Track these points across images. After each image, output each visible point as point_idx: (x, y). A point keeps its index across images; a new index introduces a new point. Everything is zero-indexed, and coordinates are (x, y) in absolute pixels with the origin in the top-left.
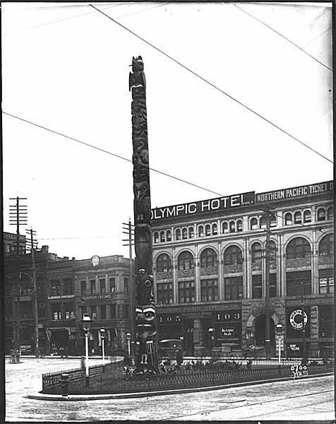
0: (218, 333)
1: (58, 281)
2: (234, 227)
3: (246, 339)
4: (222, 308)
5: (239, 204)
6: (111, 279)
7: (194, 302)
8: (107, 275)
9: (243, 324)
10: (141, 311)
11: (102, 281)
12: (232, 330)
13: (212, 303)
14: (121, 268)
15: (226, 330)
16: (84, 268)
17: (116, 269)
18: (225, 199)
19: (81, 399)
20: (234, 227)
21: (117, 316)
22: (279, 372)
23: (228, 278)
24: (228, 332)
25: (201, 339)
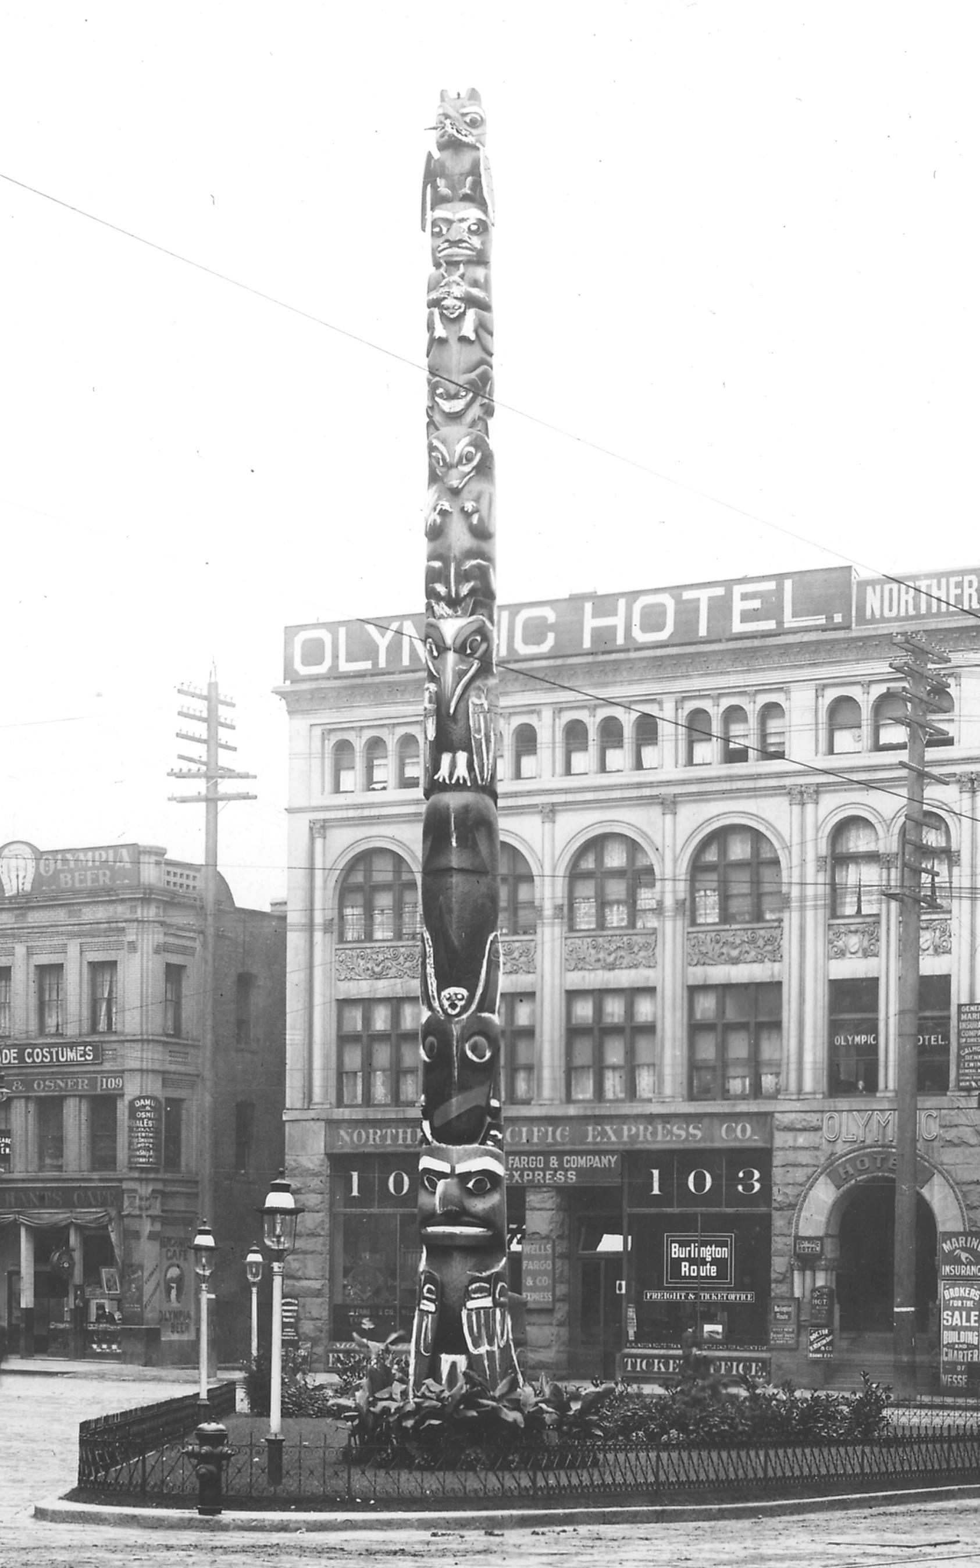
2: (745, 734)
3: (792, 1298)
4: (680, 1136)
5: (770, 625)
6: (43, 970)
7: (527, 1102)
9: (778, 1222)
12: (722, 1252)
13: (626, 1109)
14: (151, 912)
15: (693, 1251)
20: (745, 734)
21: (122, 1155)
24: (703, 1262)
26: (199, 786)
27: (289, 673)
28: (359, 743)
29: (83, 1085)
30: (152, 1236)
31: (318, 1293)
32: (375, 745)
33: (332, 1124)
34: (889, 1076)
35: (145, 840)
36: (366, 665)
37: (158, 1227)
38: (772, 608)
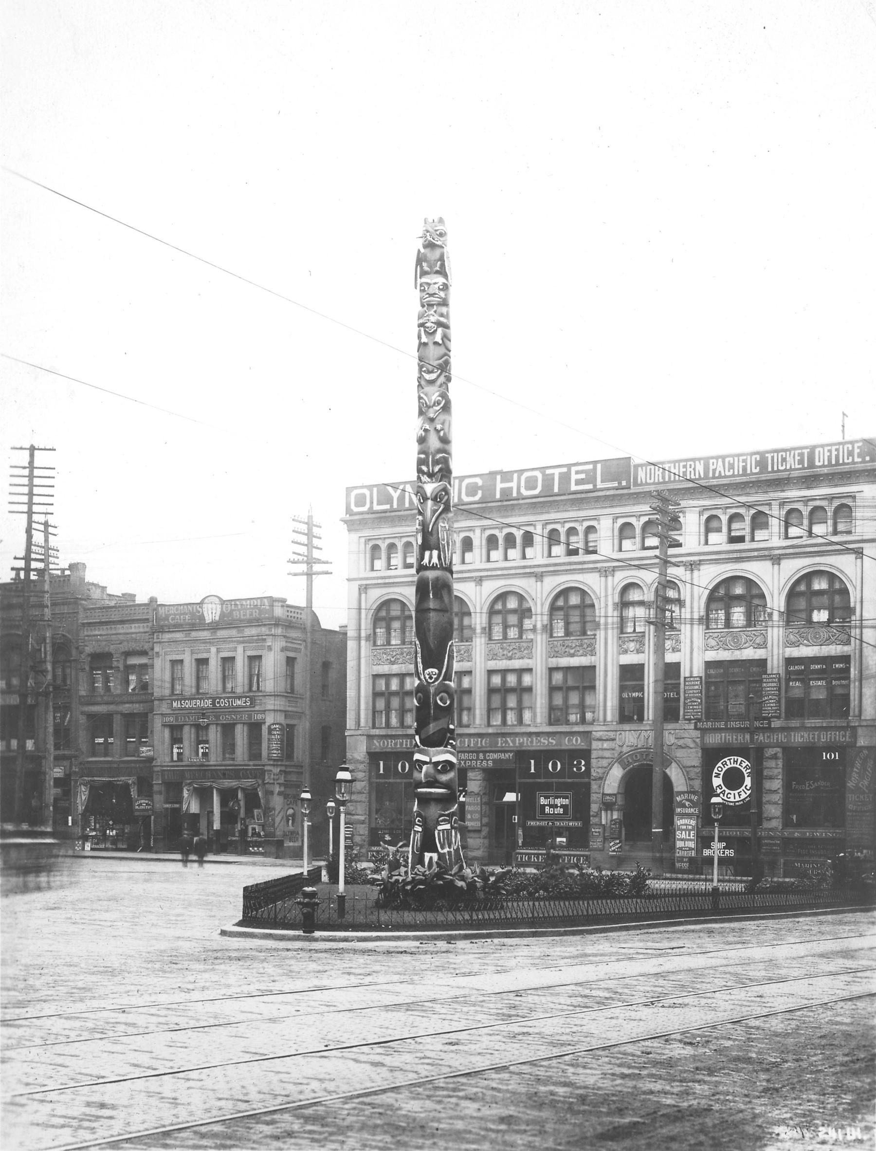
0: (528, 807)
1: (109, 656)
3: (601, 824)
7: (468, 726)
8: (240, 649)
9: (594, 786)
10: (427, 759)
11: (228, 662)
12: (566, 802)
13: (518, 730)
15: (551, 801)
16: (177, 627)
17: (264, 630)
18: (556, 472)
19: (345, 940)
22: (715, 903)
23: (557, 669)
24: (556, 806)
25: (485, 820)
26: (303, 567)
27: (349, 511)
28: (383, 546)
29: (245, 717)
30: (280, 793)
31: (363, 822)
32: (392, 547)
33: (370, 737)
34: (650, 712)
35: (276, 595)
36: (387, 507)
37: (282, 789)
38: (590, 478)
